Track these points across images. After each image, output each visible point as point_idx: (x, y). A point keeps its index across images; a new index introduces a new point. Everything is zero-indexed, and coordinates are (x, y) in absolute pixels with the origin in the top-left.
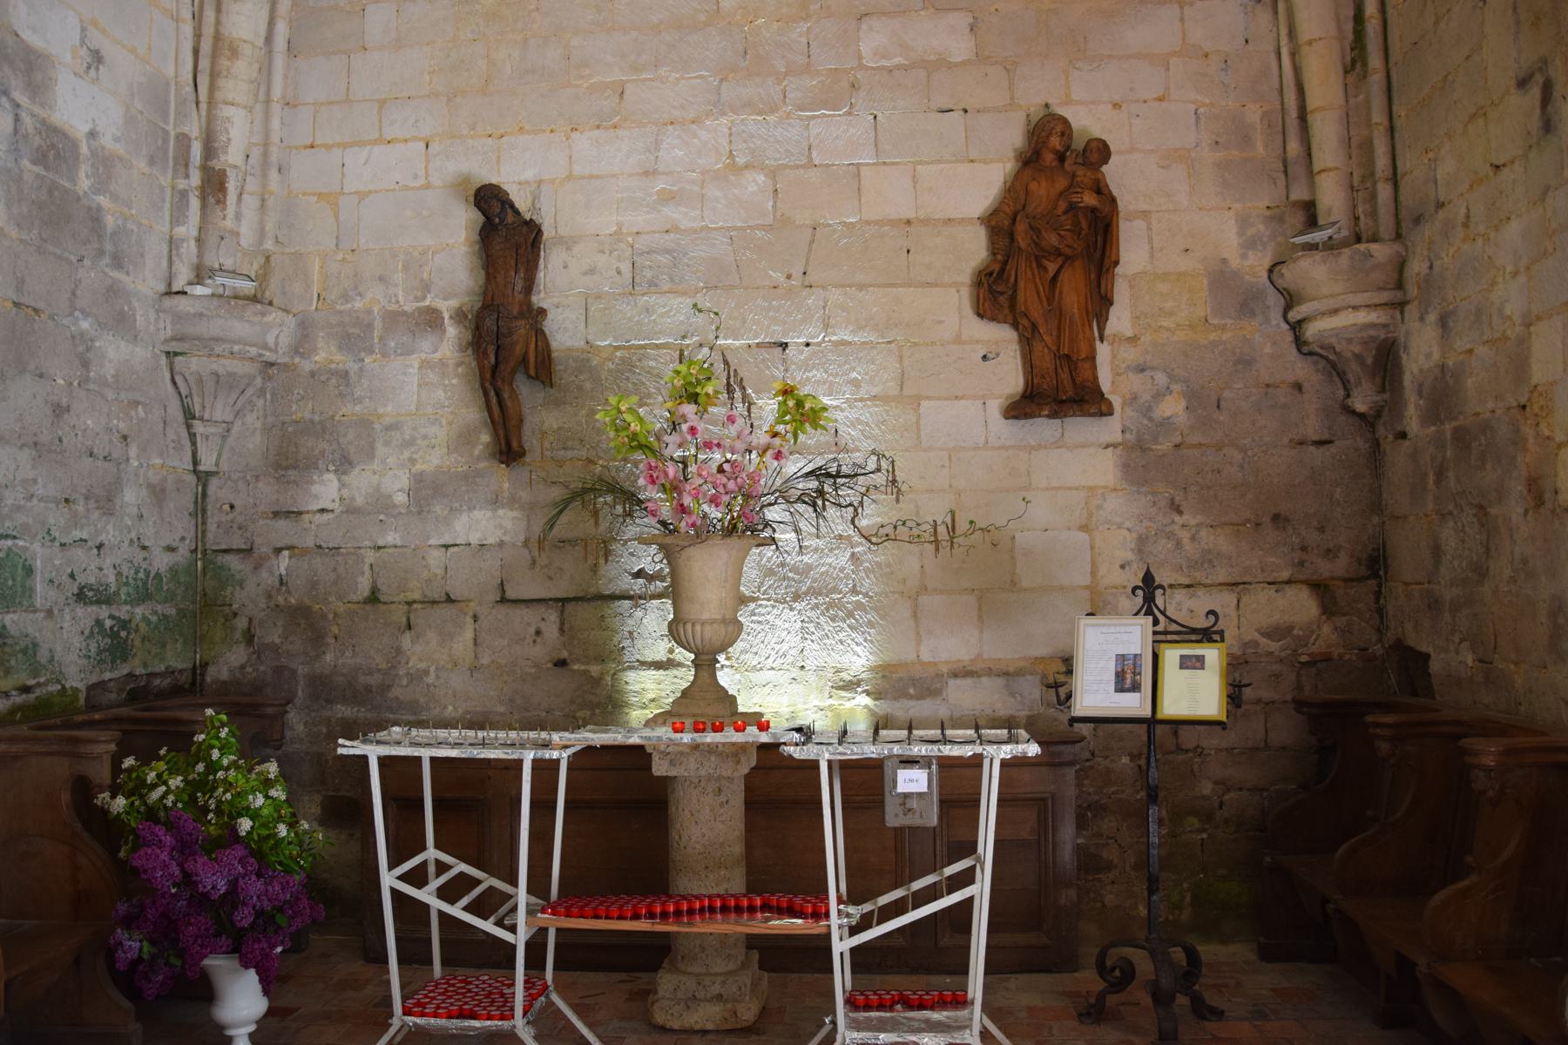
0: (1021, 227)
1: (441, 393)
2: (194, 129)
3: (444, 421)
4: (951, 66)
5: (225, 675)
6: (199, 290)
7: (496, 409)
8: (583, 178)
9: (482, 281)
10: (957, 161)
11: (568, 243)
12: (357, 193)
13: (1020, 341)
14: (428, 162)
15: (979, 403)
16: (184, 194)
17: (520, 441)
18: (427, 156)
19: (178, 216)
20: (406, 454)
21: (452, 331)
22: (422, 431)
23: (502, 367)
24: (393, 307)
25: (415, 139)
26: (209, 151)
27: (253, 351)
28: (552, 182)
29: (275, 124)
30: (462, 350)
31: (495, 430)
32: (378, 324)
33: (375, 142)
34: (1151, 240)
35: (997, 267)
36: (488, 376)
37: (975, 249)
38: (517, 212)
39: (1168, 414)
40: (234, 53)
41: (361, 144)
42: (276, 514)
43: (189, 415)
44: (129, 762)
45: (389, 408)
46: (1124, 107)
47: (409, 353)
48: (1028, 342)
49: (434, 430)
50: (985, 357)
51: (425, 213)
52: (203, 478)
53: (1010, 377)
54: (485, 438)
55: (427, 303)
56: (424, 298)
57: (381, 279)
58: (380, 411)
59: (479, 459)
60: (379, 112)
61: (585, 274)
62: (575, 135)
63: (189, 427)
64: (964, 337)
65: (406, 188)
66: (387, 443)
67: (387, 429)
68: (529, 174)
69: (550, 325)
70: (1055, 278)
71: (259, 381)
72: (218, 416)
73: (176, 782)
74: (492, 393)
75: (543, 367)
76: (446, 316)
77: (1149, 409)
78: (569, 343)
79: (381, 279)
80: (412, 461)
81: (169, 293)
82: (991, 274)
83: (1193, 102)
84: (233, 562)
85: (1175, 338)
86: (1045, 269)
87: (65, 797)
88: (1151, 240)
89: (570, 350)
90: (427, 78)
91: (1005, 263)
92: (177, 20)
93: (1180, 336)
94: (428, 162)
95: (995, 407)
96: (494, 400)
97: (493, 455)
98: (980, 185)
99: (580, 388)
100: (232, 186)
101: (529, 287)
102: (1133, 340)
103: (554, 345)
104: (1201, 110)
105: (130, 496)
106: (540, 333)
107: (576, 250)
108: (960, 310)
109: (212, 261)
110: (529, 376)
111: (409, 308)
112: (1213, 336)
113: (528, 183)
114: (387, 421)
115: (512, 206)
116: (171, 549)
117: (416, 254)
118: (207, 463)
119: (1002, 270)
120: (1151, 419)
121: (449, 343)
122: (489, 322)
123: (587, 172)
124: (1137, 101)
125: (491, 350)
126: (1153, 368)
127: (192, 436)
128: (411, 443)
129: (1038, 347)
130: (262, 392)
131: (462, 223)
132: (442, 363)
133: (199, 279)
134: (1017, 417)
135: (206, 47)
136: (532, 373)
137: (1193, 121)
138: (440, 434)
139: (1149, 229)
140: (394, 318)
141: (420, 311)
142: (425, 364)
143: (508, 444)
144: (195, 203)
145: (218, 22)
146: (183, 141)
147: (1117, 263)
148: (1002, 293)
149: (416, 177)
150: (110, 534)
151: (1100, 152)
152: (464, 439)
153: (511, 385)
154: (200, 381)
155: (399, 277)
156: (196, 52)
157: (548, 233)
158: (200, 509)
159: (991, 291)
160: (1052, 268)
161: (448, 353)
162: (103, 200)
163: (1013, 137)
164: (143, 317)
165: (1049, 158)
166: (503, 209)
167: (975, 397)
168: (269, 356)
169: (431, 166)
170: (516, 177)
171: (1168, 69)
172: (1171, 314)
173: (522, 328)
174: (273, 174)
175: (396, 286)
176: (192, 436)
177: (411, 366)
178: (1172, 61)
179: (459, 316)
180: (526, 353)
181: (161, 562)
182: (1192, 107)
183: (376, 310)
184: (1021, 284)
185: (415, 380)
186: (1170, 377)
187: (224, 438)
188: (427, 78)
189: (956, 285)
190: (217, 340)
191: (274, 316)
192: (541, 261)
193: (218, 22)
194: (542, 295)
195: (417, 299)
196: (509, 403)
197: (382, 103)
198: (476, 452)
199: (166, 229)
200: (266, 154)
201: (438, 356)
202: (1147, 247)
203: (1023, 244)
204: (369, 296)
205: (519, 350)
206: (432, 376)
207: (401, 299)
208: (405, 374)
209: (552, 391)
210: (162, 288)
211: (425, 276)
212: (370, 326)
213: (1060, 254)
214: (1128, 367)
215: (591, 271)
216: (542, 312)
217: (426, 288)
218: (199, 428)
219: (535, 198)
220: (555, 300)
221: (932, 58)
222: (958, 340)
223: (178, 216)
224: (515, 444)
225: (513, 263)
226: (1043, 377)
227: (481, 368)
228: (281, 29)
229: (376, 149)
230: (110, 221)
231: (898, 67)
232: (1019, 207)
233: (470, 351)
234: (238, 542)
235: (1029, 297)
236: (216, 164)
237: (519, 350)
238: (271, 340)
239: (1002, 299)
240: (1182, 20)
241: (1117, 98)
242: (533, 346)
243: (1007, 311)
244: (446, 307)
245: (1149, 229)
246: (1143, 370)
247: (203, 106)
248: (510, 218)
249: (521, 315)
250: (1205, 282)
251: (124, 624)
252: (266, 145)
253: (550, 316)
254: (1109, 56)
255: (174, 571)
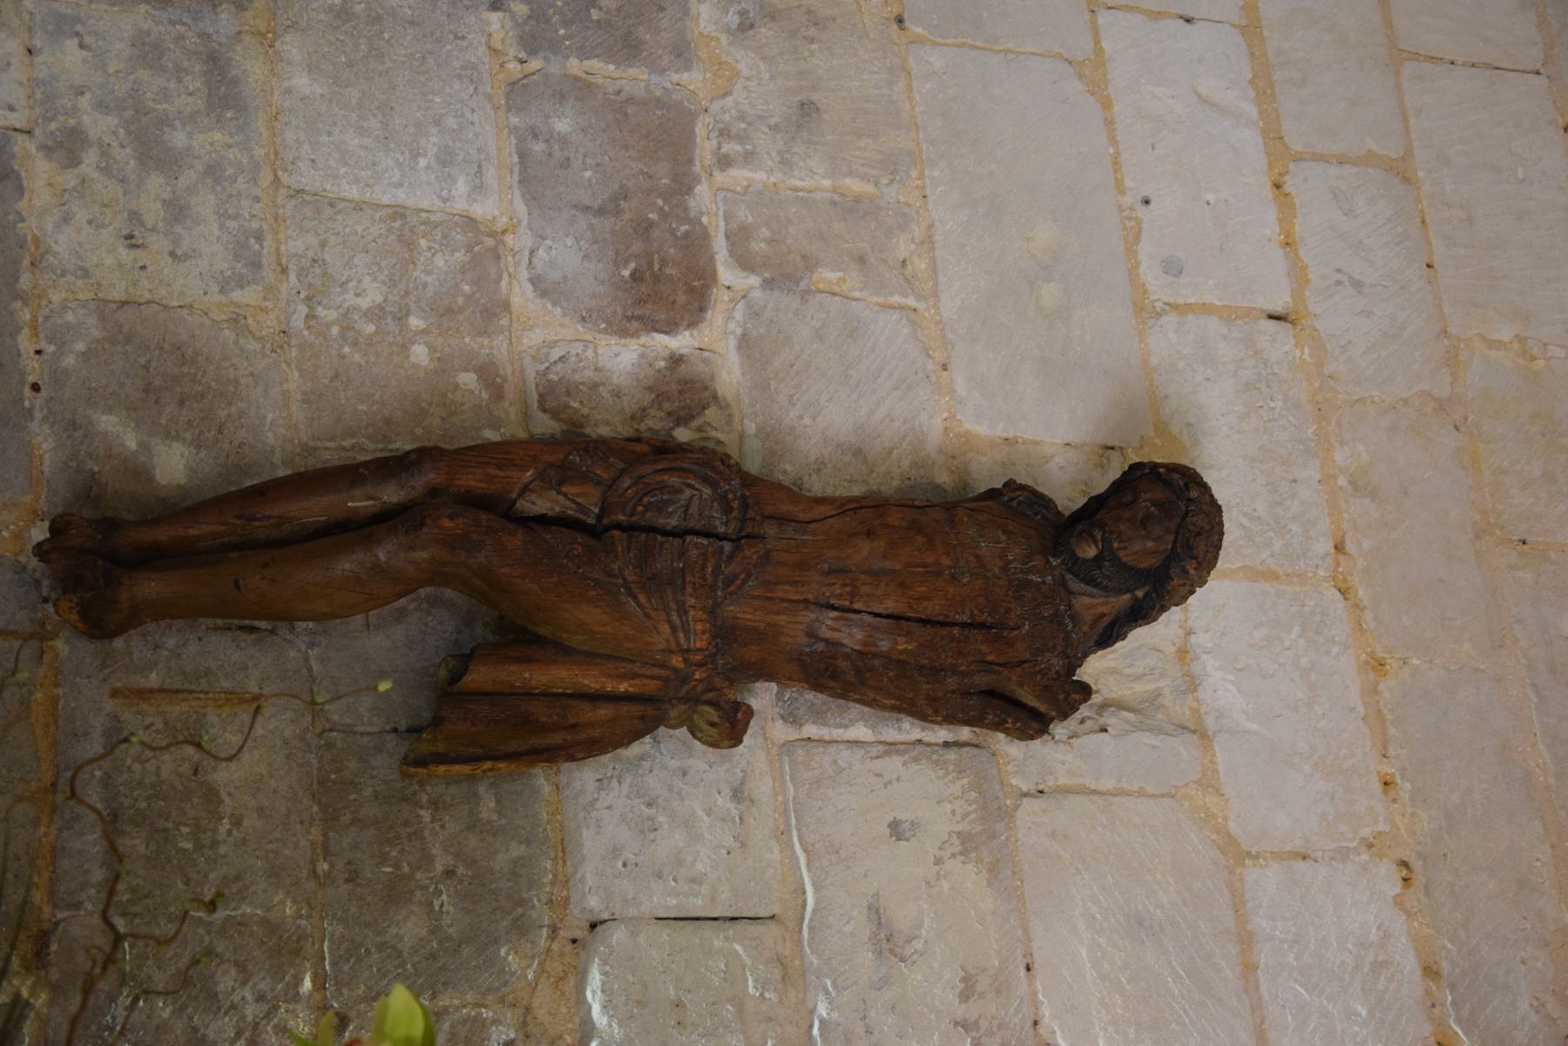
1: (372, 295)
3: (248, 296)
7: (316, 509)
8: (1239, 905)
9: (817, 486)
11: (987, 838)
12: (1100, 57)
14: (1228, 315)
17: (163, 611)
18: (1248, 313)
20: (98, 125)
21: (624, 358)
22: (204, 203)
23: (516, 540)
24: (705, 147)
25: (1298, 274)
28: (1209, 782)
30: (551, 396)
31: (219, 503)
32: (635, 79)
33: (1273, 136)
36: (470, 481)
38: (1109, 635)
41: (1263, 85)
45: (301, 82)
47: (530, 181)
49: (210, 245)
51: (1050, 293)
54: (173, 465)
55: (726, 274)
56: (745, 263)
57: (807, 109)
58: (291, 46)
59: (73, 428)
60: (1368, 159)
61: (875, 912)
62: (1386, 878)
65: (1133, 236)
66: (148, 52)
67: (215, 63)
68: (1222, 691)
69: (672, 762)
74: (391, 494)
75: (504, 715)
76: (682, 342)
78: (591, 843)
79: (807, 109)
80: (68, 147)
89: (564, 849)
90: (1505, 333)
94: (1228, 315)
96: (359, 502)
97: (89, 491)
99: (395, 894)
101: (834, 676)
103: (584, 776)
106: (642, 716)
107: (966, 877)
110: (463, 661)
111: (704, 198)
113: (1191, 684)
114: (251, 67)
115: (1141, 614)
117: (903, 246)
121: (564, 341)
122: (692, 499)
123: (1260, 923)
125: (582, 500)
128: (153, 152)
131: (1036, 421)
132: (493, 311)
136: (480, 676)
138: (193, 276)
140: (664, 136)
141: (696, 242)
142: (484, 247)
143: (152, 558)
149: (1173, 268)
152: (168, 373)
153: (436, 576)
155: (815, 177)
157: (1014, 755)
161: (532, 339)
166: (1137, 575)
169: (1213, 325)
170: (1213, 646)
173: (673, 633)
175: (786, 163)
177: (479, 188)
179: (684, 391)
180: (565, 652)
183: (693, 79)
185: (422, 198)
188: (1505, 333)
192: (909, 730)
194: (781, 732)
195: (739, 237)
196: (346, 565)
197: (1401, 171)
198: (107, 422)
201: (522, 296)
204: (743, 60)
205: (587, 618)
206: (439, 265)
207: (738, 175)
208: (446, 159)
209: (385, 766)
211: (827, 275)
212: (628, 49)
215: (888, 941)
216: (731, 726)
217: (785, 274)
219: (1142, 711)
220: (762, 787)
224: (150, 587)
225: (932, 608)
227: (502, 453)
229: (1250, 139)
231: (310, 670)
233: (545, 425)
237: (587, 618)
242: (592, 680)
244: (715, 344)
248: (1093, 604)
249: (725, 634)
253: (700, 758)
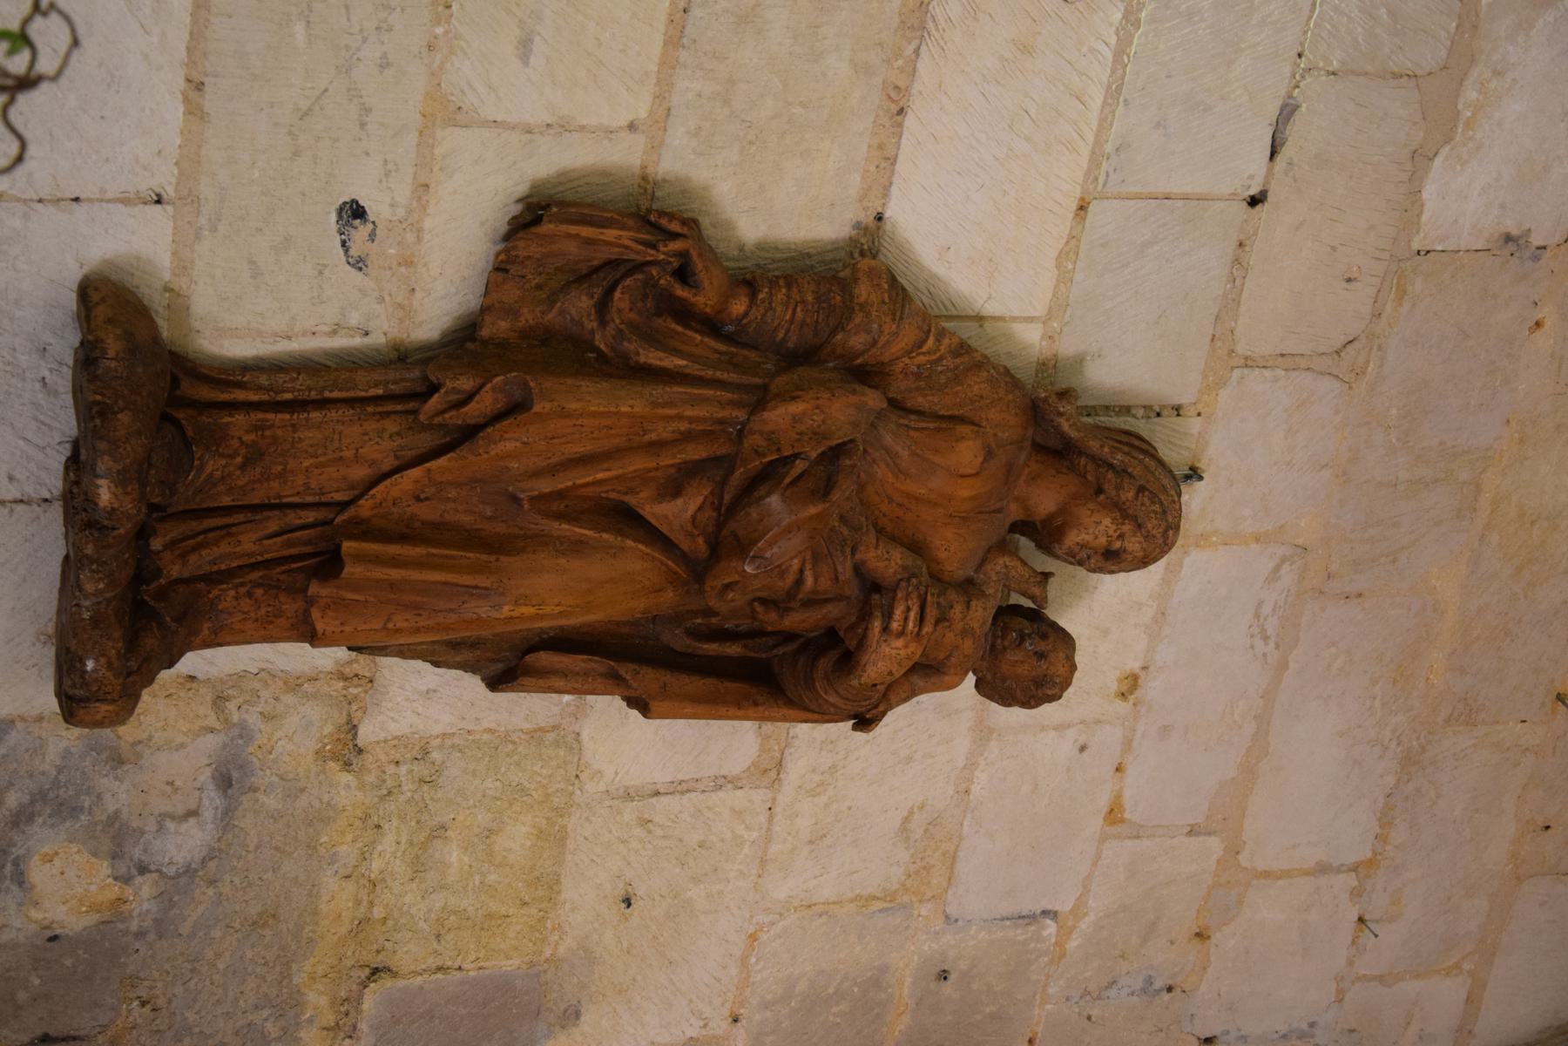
0: (840, 411)
4: (1420, 158)
10: (1096, 158)
13: (401, 356)
15: (164, 178)
34: (680, 788)
35: (705, 299)
37: (771, 199)
39: (39, 874)
46: (1122, 707)
48: (403, 383)
50: (355, 212)
53: (263, 301)
64: (449, 139)
70: (626, 519)
77: (65, 810)
82: (683, 274)
83: (1079, 909)
85: (329, 882)
86: (673, 488)
88: (680, 788)
91: (712, 326)
93: (338, 898)
95: (139, 242)
98: (999, 235)
102: (346, 748)
104: (1050, 928)
108: (562, 127)
112: (318, 1000)
119: (684, 314)
120: (22, 818)
124: (1127, 745)
126: (227, 817)
129: (372, 442)
134: (88, 359)
137: (1027, 907)
139: (722, 782)
147: (641, 705)
148: (603, 306)
151: (1024, 660)
159: (615, 269)
160: (677, 514)
163: (1124, 353)
165: (1045, 500)
167: (190, 162)
171: (1192, 831)
172: (418, 868)
178: (1215, 845)
182: (1064, 905)
184: (632, 402)
186: (189, 871)
189: (662, 115)
202: (661, 778)
203: (778, 416)
213: (715, 548)
214: (245, 733)
221: (1470, 94)
222: (442, 111)
226: (254, 456)
232: (899, 386)
235: (581, 420)
239: (580, 304)
240: (1322, 869)
241: (1152, 688)
243: (528, 317)
245: (722, 782)
246: (225, 782)
250: (510, 965)
254: (1283, 666)
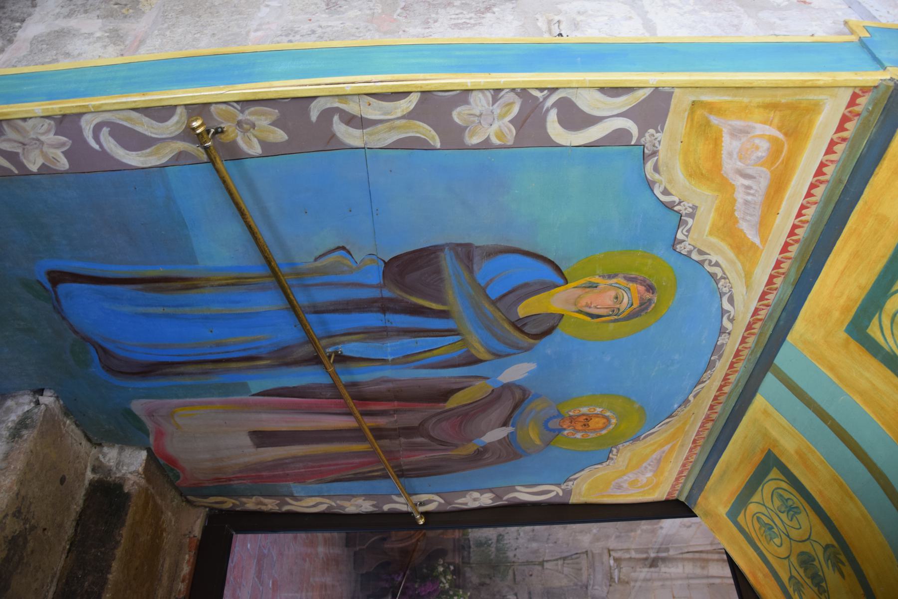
2: (672, 553)
5: (468, 575)
6: (612, 562)
16: (647, 552)
19: (636, 550)
26: (664, 560)
27: (591, 582)
29: (680, 582)
40: (703, 568)
42: (530, 593)
43: (564, 558)
44: (452, 568)
52: (541, 564)
63: (560, 559)
71: (580, 583)
72: (565, 569)
73: (447, 586)
81: (609, 551)
84: (510, 576)
87: (440, 547)
92: (711, 544)
100: (653, 569)
105: (534, 545)
109: (623, 564)
116: (515, 556)
118: (547, 565)
127: (557, 560)
130: (576, 585)
133: (615, 560)
135: (704, 556)
144: (644, 556)
145: (713, 560)
146: (667, 550)
150: (521, 541)
154: (577, 563)
156: (701, 552)
158: (528, 563)
162: (639, 532)
164: (600, 544)
168: (590, 588)
174: (660, 583)
176: (557, 560)
181: (510, 554)
187: (557, 571)
190: (594, 570)
191: (605, 589)
193: (713, 560)
199: (633, 547)
200: (667, 579)
210: (611, 548)
218: (560, 562)
223: (636, 550)
228: (718, 581)
230: (633, 534)
234: (518, 578)
236: (660, 563)
238: (596, 587)
247: (681, 556)
251: (489, 546)
252: (672, 579)
255: (507, 557)
